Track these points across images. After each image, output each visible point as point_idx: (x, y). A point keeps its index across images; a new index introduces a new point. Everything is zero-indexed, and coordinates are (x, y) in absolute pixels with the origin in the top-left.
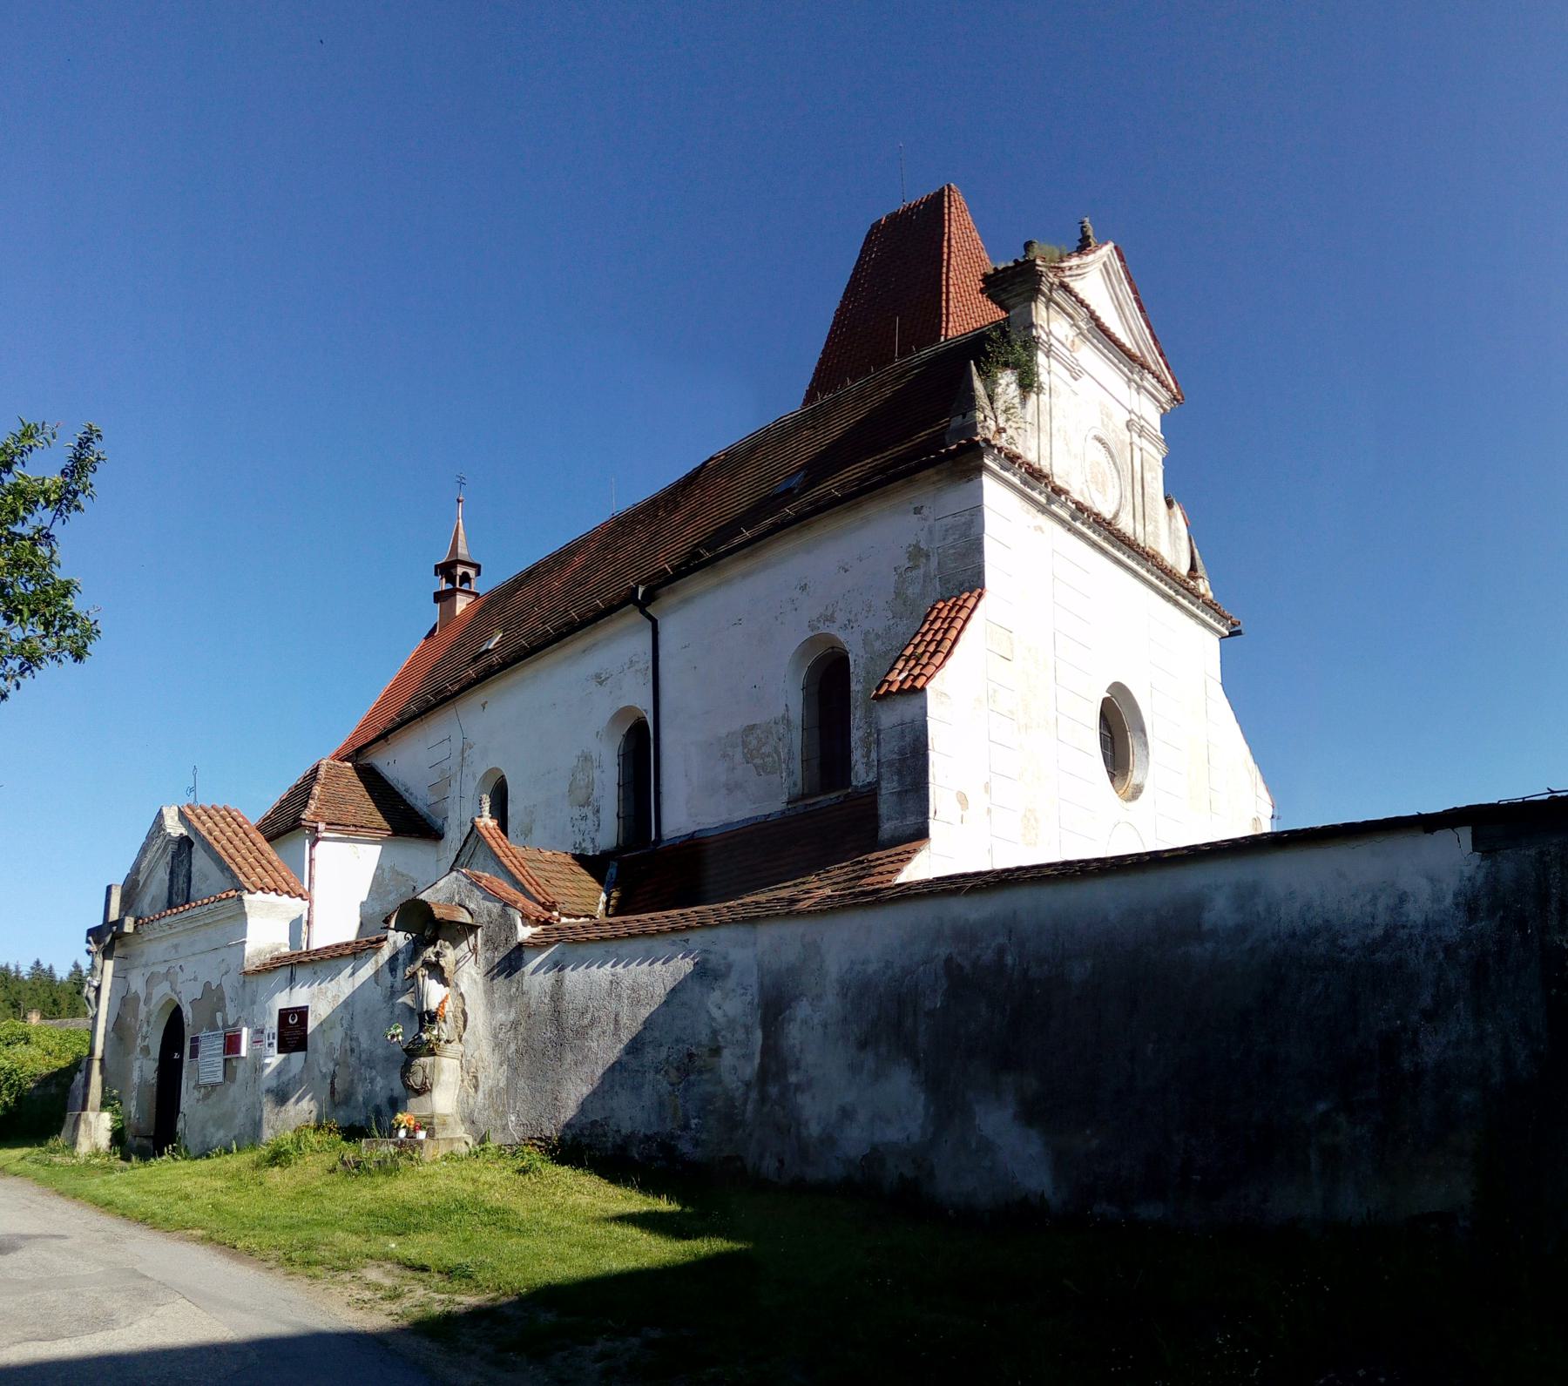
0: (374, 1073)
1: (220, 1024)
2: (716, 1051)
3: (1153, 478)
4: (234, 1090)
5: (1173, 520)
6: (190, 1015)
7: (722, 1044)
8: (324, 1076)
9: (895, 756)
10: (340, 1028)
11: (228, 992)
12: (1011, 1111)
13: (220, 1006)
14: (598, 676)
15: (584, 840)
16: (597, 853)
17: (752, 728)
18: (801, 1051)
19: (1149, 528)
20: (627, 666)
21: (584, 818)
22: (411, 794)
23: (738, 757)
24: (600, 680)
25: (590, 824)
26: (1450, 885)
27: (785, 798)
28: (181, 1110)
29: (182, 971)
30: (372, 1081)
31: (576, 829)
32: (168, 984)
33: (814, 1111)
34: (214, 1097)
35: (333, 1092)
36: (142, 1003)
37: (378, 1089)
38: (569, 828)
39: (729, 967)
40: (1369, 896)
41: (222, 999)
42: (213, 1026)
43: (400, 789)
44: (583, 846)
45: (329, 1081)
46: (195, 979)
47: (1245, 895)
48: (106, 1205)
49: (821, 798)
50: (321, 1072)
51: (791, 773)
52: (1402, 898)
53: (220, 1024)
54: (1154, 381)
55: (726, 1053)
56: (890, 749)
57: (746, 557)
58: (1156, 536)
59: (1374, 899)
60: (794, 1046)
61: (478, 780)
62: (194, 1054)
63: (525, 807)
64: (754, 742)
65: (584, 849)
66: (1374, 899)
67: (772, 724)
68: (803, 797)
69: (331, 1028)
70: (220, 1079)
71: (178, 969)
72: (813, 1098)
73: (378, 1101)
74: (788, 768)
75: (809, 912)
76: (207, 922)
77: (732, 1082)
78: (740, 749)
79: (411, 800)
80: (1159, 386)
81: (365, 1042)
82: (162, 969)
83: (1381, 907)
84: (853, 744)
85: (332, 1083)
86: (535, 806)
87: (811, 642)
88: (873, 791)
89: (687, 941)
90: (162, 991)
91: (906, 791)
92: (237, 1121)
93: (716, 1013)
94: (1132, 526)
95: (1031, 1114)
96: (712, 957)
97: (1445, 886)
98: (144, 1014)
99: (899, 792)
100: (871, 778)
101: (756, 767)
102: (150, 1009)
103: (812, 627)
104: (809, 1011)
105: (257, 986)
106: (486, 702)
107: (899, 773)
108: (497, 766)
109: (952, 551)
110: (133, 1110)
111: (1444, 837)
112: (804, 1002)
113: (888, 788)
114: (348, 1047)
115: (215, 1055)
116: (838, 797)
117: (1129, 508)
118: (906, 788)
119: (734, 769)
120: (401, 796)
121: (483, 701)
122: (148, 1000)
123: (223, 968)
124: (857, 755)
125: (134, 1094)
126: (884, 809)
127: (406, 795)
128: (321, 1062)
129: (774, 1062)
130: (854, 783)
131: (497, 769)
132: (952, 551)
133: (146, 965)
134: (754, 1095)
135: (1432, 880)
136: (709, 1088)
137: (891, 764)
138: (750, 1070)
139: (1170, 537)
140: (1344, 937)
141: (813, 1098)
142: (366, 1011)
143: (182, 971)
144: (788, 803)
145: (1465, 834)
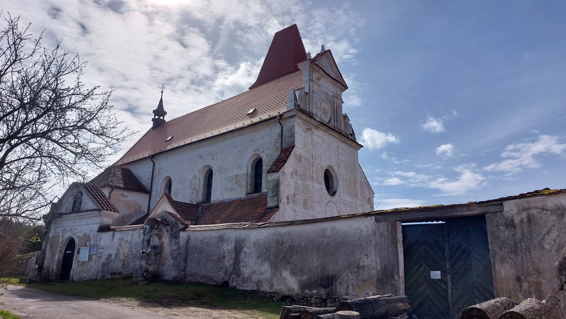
0: (136, 260)
1: (88, 245)
2: (224, 257)
3: (339, 110)
4: (92, 263)
5: (345, 120)
6: (78, 242)
7: (225, 256)
8: (121, 260)
9: (271, 187)
10: (127, 249)
11: (92, 237)
12: (289, 272)
13: (89, 240)
14: (200, 156)
15: (192, 199)
16: (196, 203)
17: (237, 175)
18: (244, 258)
19: (339, 123)
20: (208, 154)
21: (193, 193)
22: (142, 179)
23: (234, 182)
24: (201, 157)
25: (195, 195)
26: (371, 228)
27: (245, 194)
28: (72, 268)
29: (76, 229)
30: (136, 262)
31: (190, 196)
32: (71, 233)
33: (246, 271)
34: (84, 265)
35: (124, 264)
36: (60, 237)
37: (137, 264)
38: (189, 196)
39: (229, 239)
40: (355, 230)
41: (90, 238)
42: (86, 245)
43: (138, 177)
44: (192, 200)
45: (123, 262)
46: (81, 232)
47: (333, 229)
48: (79, 295)
49: (254, 195)
50: (120, 259)
51: (247, 188)
52: (361, 231)
53: (88, 245)
54: (340, 84)
55: (226, 258)
56: (271, 185)
57: (239, 131)
58: (341, 125)
59: (356, 231)
60: (242, 257)
61: (163, 179)
62: (78, 252)
63: (176, 188)
64: (238, 179)
65: (192, 202)
66: (356, 231)
67: (243, 175)
68: (250, 194)
69: (125, 248)
70: (87, 260)
71: (74, 229)
72: (246, 268)
73: (137, 267)
74: (246, 186)
75: (247, 228)
76: (86, 216)
77: (228, 264)
78: (234, 180)
79: (141, 181)
80: (341, 85)
81: (134, 252)
82: (69, 228)
83: (357, 233)
84: (262, 182)
85: (124, 262)
86: (179, 188)
87: (254, 155)
88: (266, 195)
89: (220, 232)
90: (68, 235)
91: (274, 196)
92: (92, 271)
93: (225, 249)
94: (334, 123)
95: (293, 273)
96: (224, 236)
97: (369, 229)
98: (61, 241)
99: (272, 196)
100: (266, 191)
101: (238, 185)
102: (63, 240)
103: (254, 151)
104: (246, 250)
105: (102, 235)
106: (167, 157)
107: (272, 191)
108: (170, 176)
109: (287, 136)
110: (55, 268)
111: (369, 218)
112: (245, 248)
113: (270, 195)
114: (129, 253)
115: (87, 254)
116: (258, 195)
117: (333, 119)
118: (274, 195)
119: (233, 185)
120: (138, 180)
121: (166, 157)
122: (62, 237)
123: (91, 230)
124: (263, 185)
125: (56, 263)
126: (268, 200)
127: (139, 179)
128: (121, 256)
129: (237, 261)
130: (262, 192)
131: (169, 176)
132: (287, 136)
133: (63, 227)
134: (232, 268)
135: (367, 227)
136: (222, 266)
137: (271, 189)
138: (231, 262)
139: (344, 125)
140: (351, 238)
141: (246, 268)
142: (135, 244)
143: (76, 229)
144: (246, 195)
145: (373, 217)
